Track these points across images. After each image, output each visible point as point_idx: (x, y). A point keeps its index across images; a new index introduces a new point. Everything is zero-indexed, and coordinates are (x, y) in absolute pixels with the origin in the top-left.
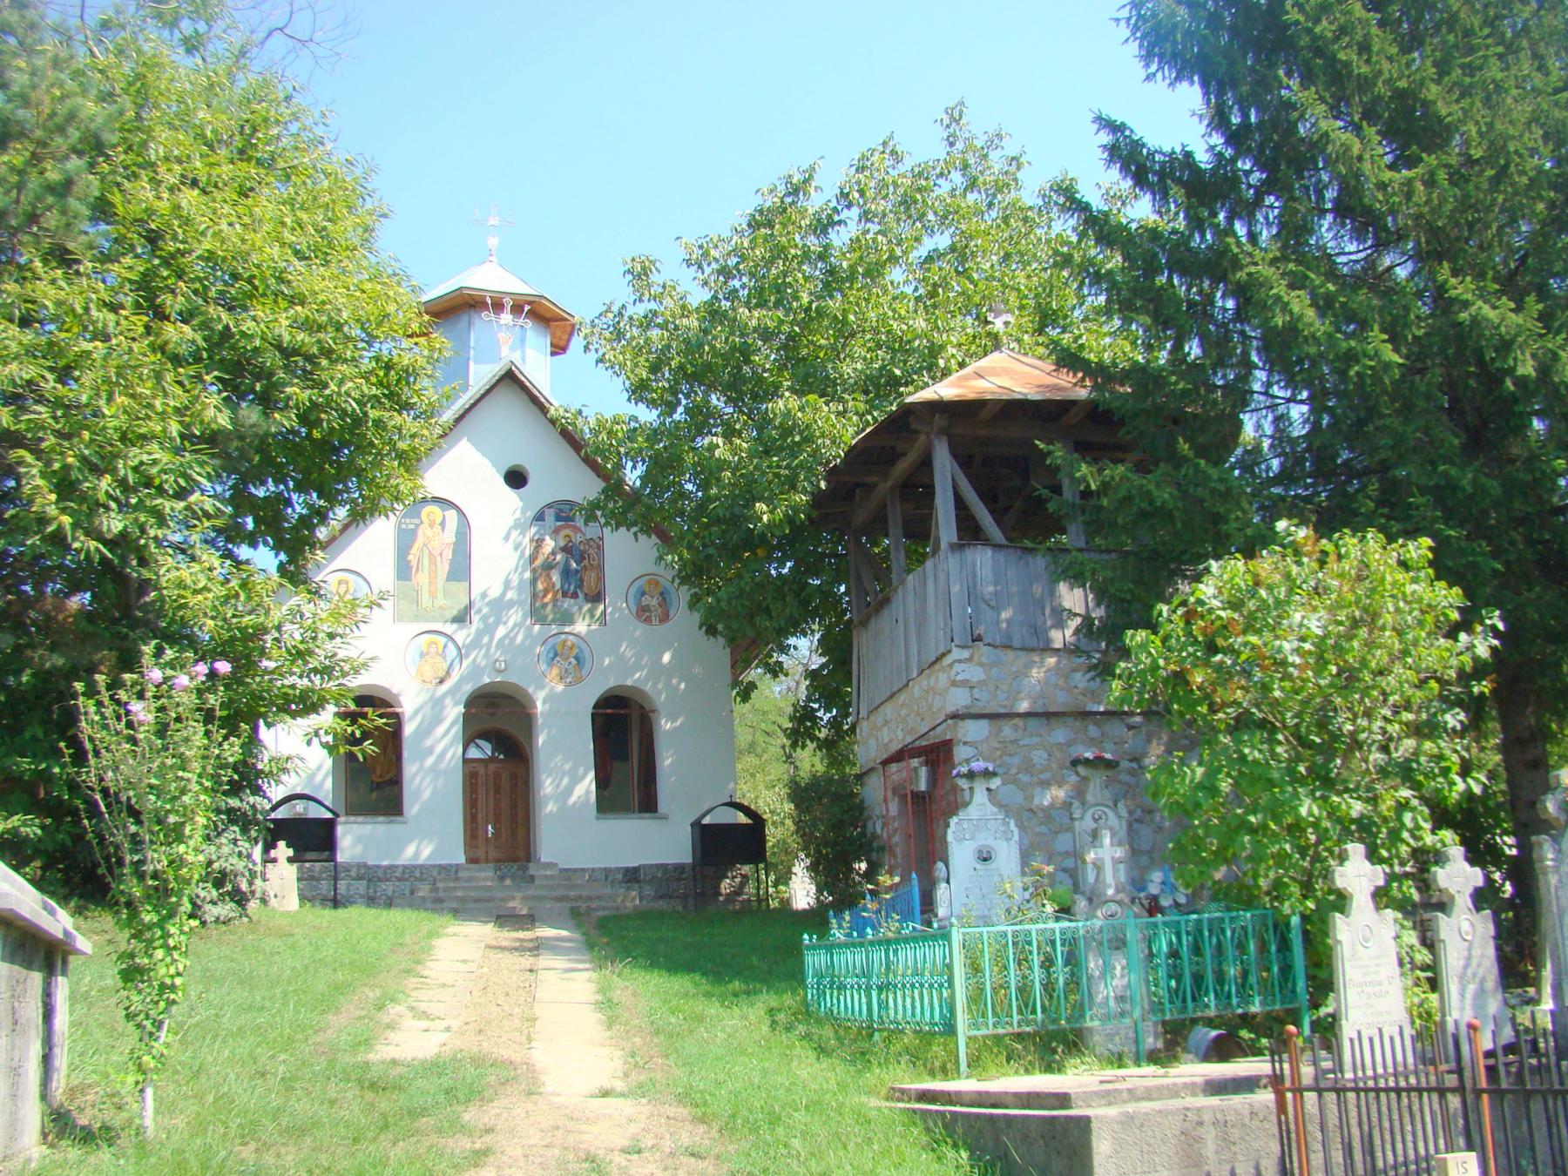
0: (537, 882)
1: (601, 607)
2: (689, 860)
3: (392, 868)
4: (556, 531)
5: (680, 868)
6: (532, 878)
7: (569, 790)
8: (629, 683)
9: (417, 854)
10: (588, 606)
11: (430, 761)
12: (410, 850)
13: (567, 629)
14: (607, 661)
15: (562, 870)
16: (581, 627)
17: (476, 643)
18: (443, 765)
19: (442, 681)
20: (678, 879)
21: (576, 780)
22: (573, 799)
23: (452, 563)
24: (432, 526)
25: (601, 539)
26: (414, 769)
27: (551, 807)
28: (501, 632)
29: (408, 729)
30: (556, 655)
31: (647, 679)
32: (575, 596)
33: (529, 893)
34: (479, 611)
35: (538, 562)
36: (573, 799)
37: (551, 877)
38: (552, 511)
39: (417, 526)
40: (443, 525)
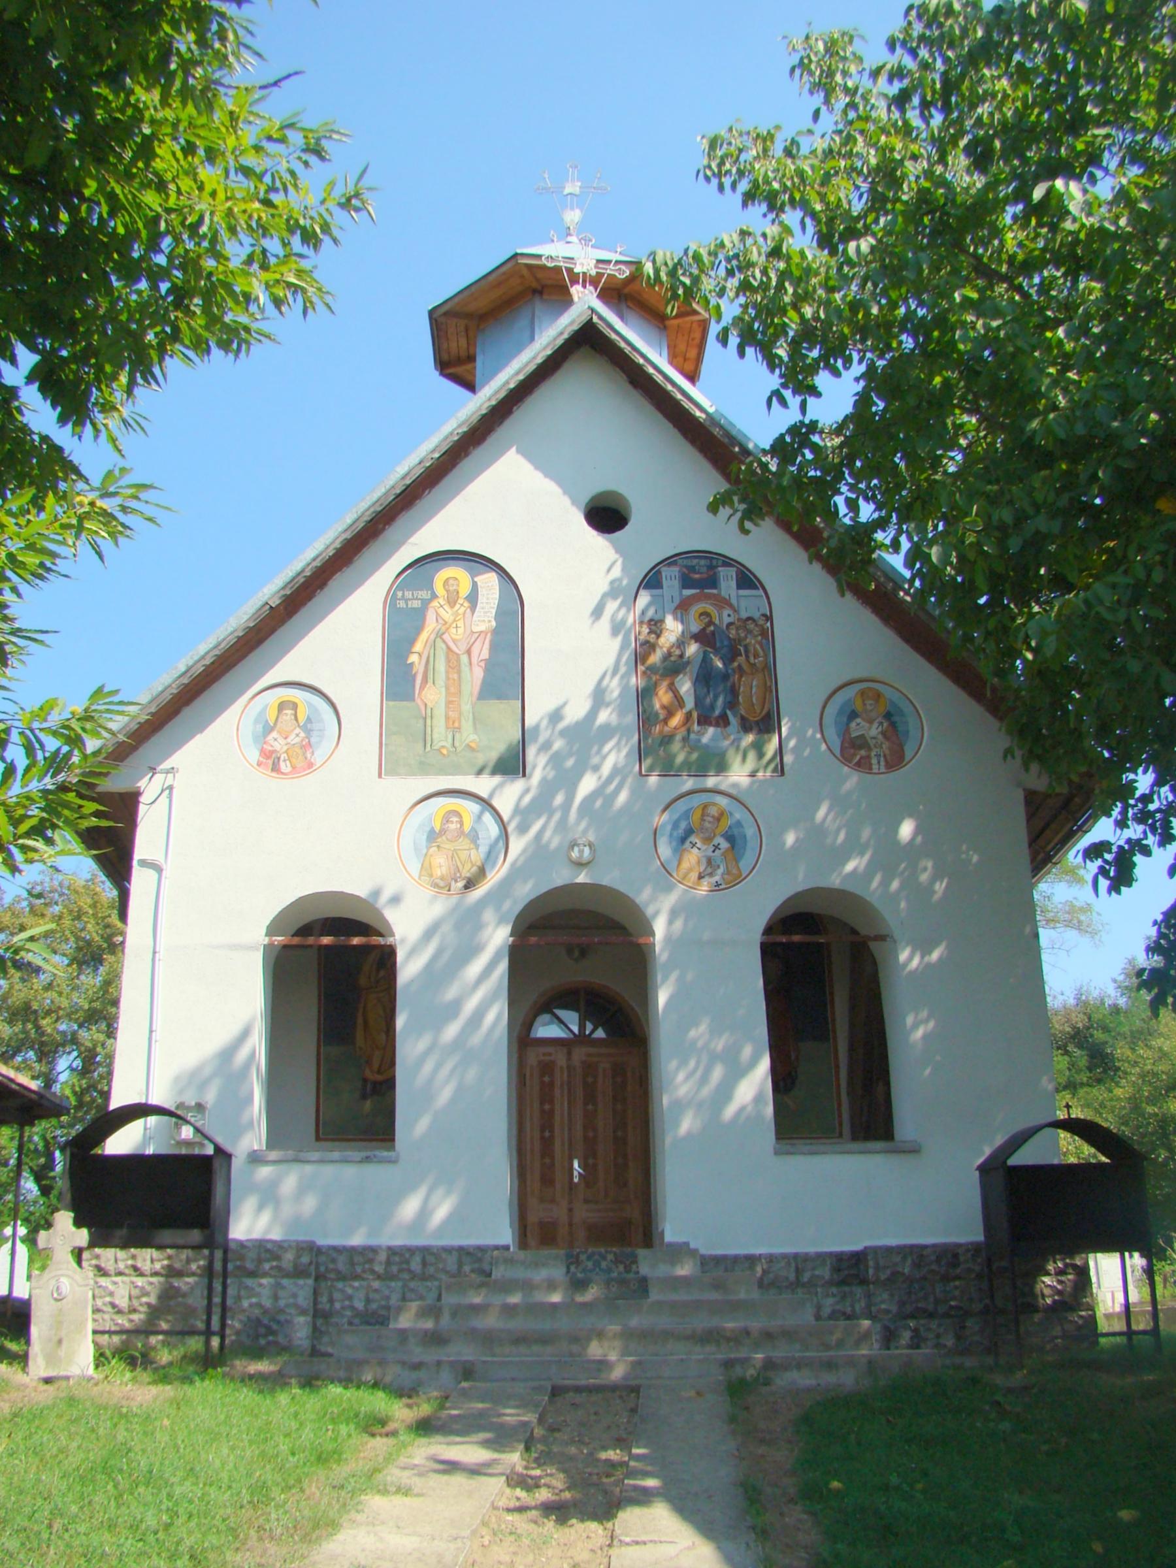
0: (655, 1295)
1: (775, 740)
2: (974, 1233)
3: (367, 1253)
4: (682, 609)
5: (949, 1255)
6: (643, 1285)
7: (725, 1092)
8: (835, 881)
9: (424, 1213)
10: (750, 738)
11: (452, 1031)
12: (410, 1207)
13: (711, 782)
14: (790, 839)
15: (710, 1263)
16: (738, 775)
17: (540, 805)
18: (476, 1039)
19: (470, 885)
20: (946, 1278)
21: (737, 1072)
22: (730, 1111)
23: (490, 667)
24: (452, 601)
25: (769, 618)
26: (422, 1045)
27: (687, 1124)
28: (587, 784)
29: (408, 970)
30: (689, 832)
31: (868, 874)
32: (723, 721)
33: (634, 1322)
34: (546, 746)
35: (655, 658)
36: (730, 1111)
37: (686, 1281)
38: (674, 571)
39: (426, 603)
40: (473, 598)
